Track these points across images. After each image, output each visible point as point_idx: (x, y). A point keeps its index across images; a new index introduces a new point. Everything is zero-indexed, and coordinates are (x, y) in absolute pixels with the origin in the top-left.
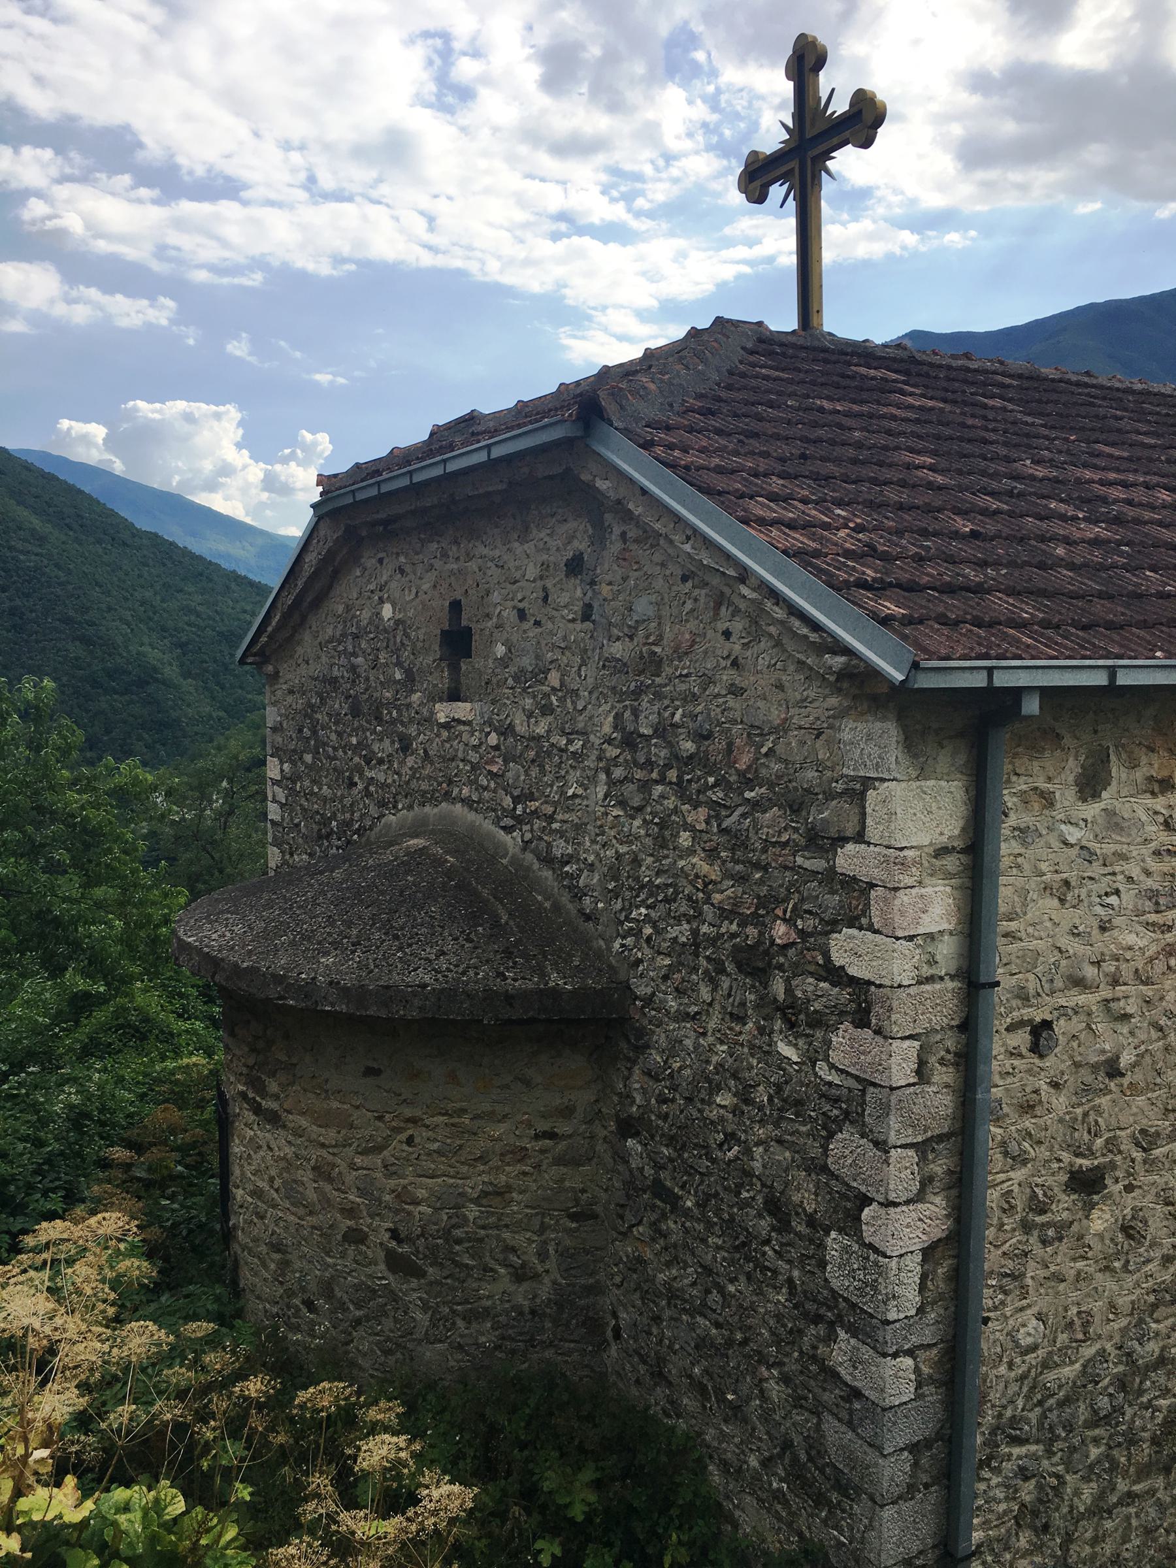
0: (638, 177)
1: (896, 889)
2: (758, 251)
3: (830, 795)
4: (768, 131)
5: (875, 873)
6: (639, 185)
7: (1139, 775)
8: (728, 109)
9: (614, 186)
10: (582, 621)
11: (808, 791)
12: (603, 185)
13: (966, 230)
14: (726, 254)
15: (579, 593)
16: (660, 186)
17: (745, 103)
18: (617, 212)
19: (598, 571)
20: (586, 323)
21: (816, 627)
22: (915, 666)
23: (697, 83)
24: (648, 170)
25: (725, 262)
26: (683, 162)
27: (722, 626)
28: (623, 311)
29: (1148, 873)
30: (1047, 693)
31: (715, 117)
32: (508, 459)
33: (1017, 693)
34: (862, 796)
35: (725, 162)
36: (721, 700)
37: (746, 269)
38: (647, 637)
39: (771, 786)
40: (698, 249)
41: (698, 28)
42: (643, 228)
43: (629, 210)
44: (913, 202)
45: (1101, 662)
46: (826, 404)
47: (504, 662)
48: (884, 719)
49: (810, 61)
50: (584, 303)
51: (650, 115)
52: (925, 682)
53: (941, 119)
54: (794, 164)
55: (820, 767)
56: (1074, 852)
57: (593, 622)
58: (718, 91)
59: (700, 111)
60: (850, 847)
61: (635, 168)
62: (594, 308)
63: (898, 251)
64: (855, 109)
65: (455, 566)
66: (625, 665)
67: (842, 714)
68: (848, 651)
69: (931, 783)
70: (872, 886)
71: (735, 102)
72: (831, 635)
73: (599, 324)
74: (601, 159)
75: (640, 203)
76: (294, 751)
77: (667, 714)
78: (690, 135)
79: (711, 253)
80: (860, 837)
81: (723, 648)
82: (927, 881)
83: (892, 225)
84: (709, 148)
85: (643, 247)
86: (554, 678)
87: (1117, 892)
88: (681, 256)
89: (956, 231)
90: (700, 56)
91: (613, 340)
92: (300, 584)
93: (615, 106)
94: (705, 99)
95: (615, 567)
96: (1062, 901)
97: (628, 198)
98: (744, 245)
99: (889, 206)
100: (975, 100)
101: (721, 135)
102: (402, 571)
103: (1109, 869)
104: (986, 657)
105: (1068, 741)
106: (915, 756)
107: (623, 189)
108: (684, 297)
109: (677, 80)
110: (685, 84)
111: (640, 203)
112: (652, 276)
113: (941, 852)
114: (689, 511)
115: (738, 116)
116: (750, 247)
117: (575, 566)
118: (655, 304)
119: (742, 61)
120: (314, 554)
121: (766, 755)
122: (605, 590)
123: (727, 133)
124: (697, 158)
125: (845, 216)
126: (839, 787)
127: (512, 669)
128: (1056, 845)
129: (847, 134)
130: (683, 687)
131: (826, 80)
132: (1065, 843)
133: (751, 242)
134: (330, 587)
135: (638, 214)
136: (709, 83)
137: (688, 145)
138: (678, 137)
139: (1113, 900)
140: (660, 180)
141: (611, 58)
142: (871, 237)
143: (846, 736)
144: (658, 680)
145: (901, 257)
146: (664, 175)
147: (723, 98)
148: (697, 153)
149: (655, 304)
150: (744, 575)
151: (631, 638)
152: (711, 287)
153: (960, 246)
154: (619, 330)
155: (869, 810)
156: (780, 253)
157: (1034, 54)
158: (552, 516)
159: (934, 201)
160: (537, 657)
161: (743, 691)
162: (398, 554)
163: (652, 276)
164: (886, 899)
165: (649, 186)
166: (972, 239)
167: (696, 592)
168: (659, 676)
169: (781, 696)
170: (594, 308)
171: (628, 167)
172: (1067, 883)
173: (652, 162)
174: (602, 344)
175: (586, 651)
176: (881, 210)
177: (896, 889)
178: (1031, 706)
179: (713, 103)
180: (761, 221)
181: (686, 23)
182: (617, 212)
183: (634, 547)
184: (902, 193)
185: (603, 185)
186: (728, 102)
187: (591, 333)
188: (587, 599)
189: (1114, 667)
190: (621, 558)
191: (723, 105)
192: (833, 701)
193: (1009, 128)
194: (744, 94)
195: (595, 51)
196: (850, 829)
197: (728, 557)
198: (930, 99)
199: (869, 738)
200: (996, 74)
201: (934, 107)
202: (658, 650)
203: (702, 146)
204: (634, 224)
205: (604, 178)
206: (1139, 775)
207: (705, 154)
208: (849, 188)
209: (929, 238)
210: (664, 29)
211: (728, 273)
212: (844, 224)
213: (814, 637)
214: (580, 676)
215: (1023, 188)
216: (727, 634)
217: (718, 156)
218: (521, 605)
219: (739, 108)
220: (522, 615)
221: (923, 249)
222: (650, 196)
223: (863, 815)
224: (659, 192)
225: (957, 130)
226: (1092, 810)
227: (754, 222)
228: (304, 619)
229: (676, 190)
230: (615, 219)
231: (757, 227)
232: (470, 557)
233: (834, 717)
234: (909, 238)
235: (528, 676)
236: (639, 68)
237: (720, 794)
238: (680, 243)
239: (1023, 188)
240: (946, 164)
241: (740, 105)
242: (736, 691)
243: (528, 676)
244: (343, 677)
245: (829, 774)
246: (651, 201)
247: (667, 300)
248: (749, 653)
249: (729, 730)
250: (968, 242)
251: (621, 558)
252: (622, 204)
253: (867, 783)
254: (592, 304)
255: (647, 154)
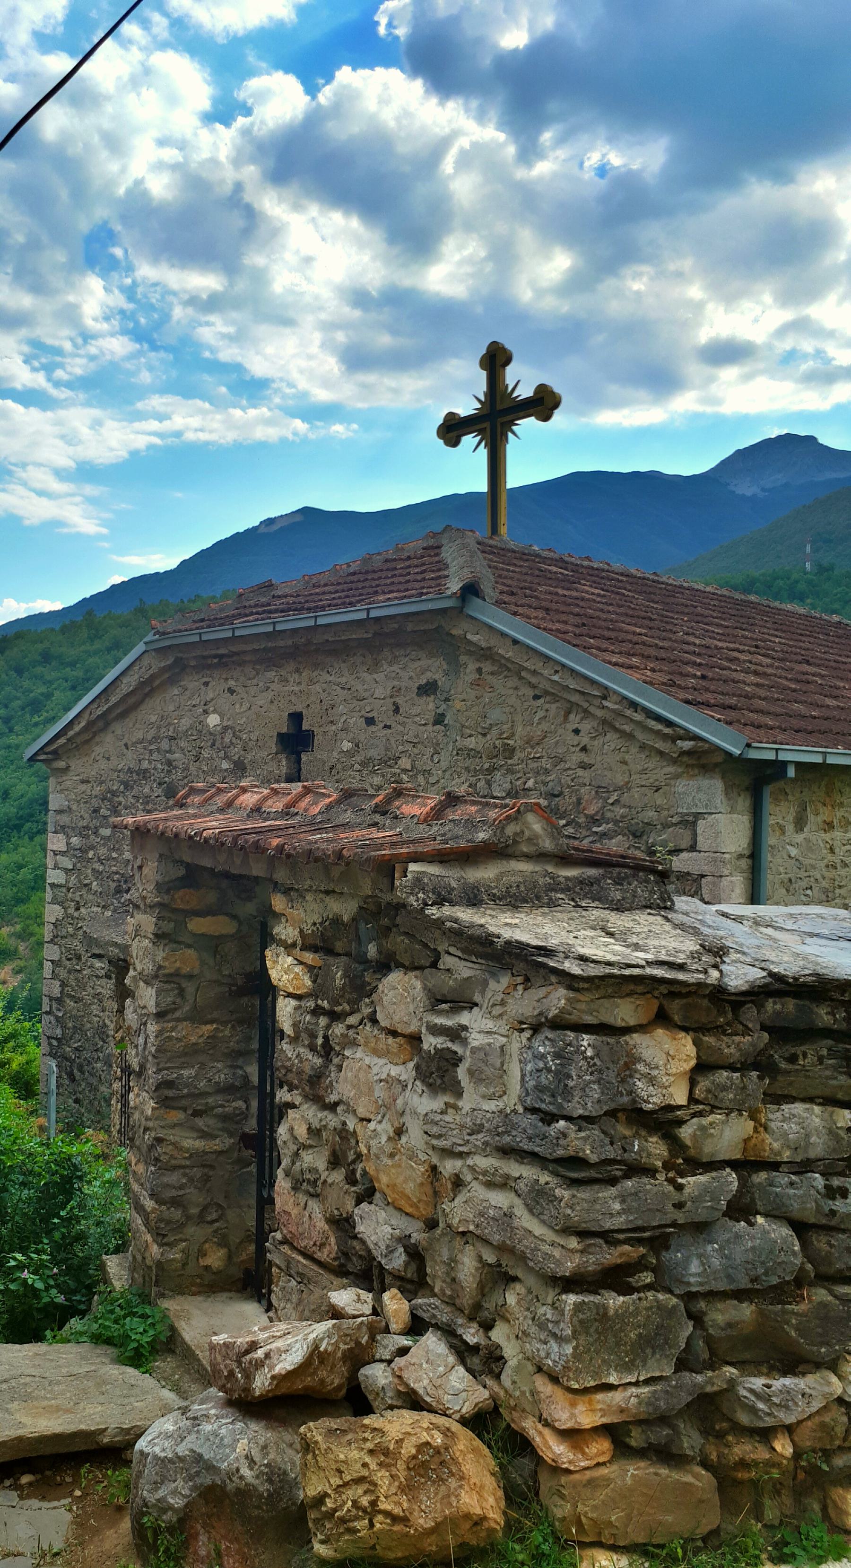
0: (58, 351)
1: (721, 876)
2: (167, 426)
3: (666, 826)
4: (178, 322)
5: (706, 869)
6: (58, 359)
7: (820, 819)
8: (144, 300)
9: (35, 357)
10: (434, 725)
11: (648, 824)
12: (25, 355)
13: (349, 423)
14: (137, 425)
15: (431, 706)
16: (79, 361)
17: (158, 296)
18: (39, 380)
19: (452, 692)
20: (7, 477)
21: (669, 724)
22: (748, 745)
23: (115, 275)
24: (68, 346)
25: (138, 433)
26: (101, 342)
27: (571, 726)
28: (42, 468)
29: (824, 878)
30: (799, 765)
31: (131, 306)
32: (377, 619)
33: (785, 764)
34: (694, 824)
35: (138, 346)
36: (571, 772)
37: (157, 441)
38: (501, 734)
39: (616, 823)
40: (113, 419)
41: (118, 228)
42: (62, 396)
43: (49, 379)
44: (305, 395)
45: (820, 750)
46: (560, 591)
47: (350, 754)
48: (712, 778)
49: (500, 360)
50: (5, 458)
51: (71, 298)
52: (753, 755)
53: (328, 327)
54: (487, 425)
55: (658, 809)
56: (793, 861)
57: (445, 726)
58: (135, 284)
59: (118, 300)
60: (684, 855)
61: (56, 343)
62: (16, 465)
63: (291, 437)
64: (538, 396)
65: (296, 689)
66: (479, 752)
67: (677, 777)
68: (696, 738)
69: (735, 816)
70: (703, 876)
71: (149, 295)
72: (685, 729)
73: (19, 479)
74: (23, 332)
75: (59, 374)
76: (87, 828)
77: (518, 783)
78: (107, 319)
79: (124, 424)
80: (693, 848)
81: (573, 739)
82: (734, 873)
83: (286, 414)
84: (124, 332)
85: (62, 413)
86: (405, 763)
87: (811, 888)
88: (96, 424)
89: (341, 423)
90: (118, 252)
91: (33, 494)
92: (114, 700)
93: (38, 288)
94: (123, 289)
95: (469, 690)
96: (788, 891)
97: (48, 369)
98: (155, 419)
99: (284, 397)
100: (357, 314)
101: (137, 323)
102: (231, 691)
103: (807, 874)
104: (775, 743)
105: (790, 797)
106: (729, 799)
107: (44, 360)
108: (101, 461)
109: (97, 270)
110: (104, 274)
111: (59, 374)
112: (70, 439)
113: (740, 856)
114: (562, 656)
115: (152, 307)
116: (161, 422)
117: (428, 689)
118: (72, 464)
119: (155, 260)
120: (136, 676)
121: (612, 804)
122: (458, 705)
123: (143, 321)
124: (114, 340)
125: (244, 402)
126: (675, 820)
127: (358, 758)
128: (786, 857)
129: (531, 411)
130: (535, 765)
131: (511, 374)
132: (790, 856)
133: (161, 417)
134: (141, 702)
135: (57, 384)
136: (126, 277)
137: (105, 326)
138: (95, 319)
139: (809, 892)
140: (79, 356)
141: (33, 245)
142: (268, 422)
143: (680, 789)
144: (510, 762)
145: (293, 441)
146: (81, 352)
147: (140, 290)
148: (113, 335)
149: (72, 464)
150: (606, 693)
151: (484, 735)
152: (124, 454)
153: (344, 437)
154: (38, 486)
155: (699, 831)
156: (188, 428)
157: (406, 280)
158: (406, 656)
159: (322, 395)
160: (387, 749)
161: (591, 766)
162: (227, 679)
163: (70, 439)
164: (714, 883)
165: (68, 360)
166: (355, 431)
167: (547, 706)
168: (511, 758)
169: (625, 767)
170: (16, 465)
171: (50, 341)
172: (790, 880)
173: (72, 340)
174: (22, 497)
175: (438, 744)
176: (277, 400)
177: (721, 876)
178: (791, 772)
179: (130, 293)
180: (170, 400)
181: (106, 223)
182: (39, 380)
183: (489, 678)
184: (294, 386)
185: (25, 355)
186: (145, 296)
187: (12, 486)
188: (439, 711)
189: (825, 753)
190: (475, 684)
191: (139, 296)
192: (671, 769)
193: (385, 340)
194: (158, 288)
195: (20, 238)
196: (684, 844)
197: (593, 682)
198: (321, 309)
199: (699, 789)
200: (374, 293)
201: (323, 316)
202: (511, 742)
203: (117, 328)
204: (54, 392)
205: (26, 349)
206: (820, 819)
207: (121, 338)
208: (248, 378)
209: (317, 427)
210: (84, 225)
211: (141, 442)
212: (243, 409)
213: (667, 730)
214: (432, 761)
215: (396, 391)
216: (577, 732)
217: (131, 340)
218: (370, 715)
219: (154, 301)
220: (370, 721)
221: (312, 436)
222: (69, 369)
223: (695, 835)
224: (77, 367)
225: (341, 337)
226: (800, 838)
227: (164, 400)
228: (107, 725)
229: (93, 366)
230: (36, 386)
231: (164, 404)
232: (312, 682)
233: (670, 779)
234: (299, 425)
235: (376, 762)
236: (61, 257)
237: (572, 831)
238: (96, 412)
239: (396, 391)
240: (332, 364)
241: (154, 298)
242: (584, 766)
243: (376, 762)
244: (155, 769)
245: (666, 813)
246: (70, 374)
247: (84, 463)
248: (596, 743)
249: (578, 790)
250: (351, 434)
251: (475, 684)
252: (42, 373)
253: (698, 816)
254: (13, 460)
255: (66, 332)
